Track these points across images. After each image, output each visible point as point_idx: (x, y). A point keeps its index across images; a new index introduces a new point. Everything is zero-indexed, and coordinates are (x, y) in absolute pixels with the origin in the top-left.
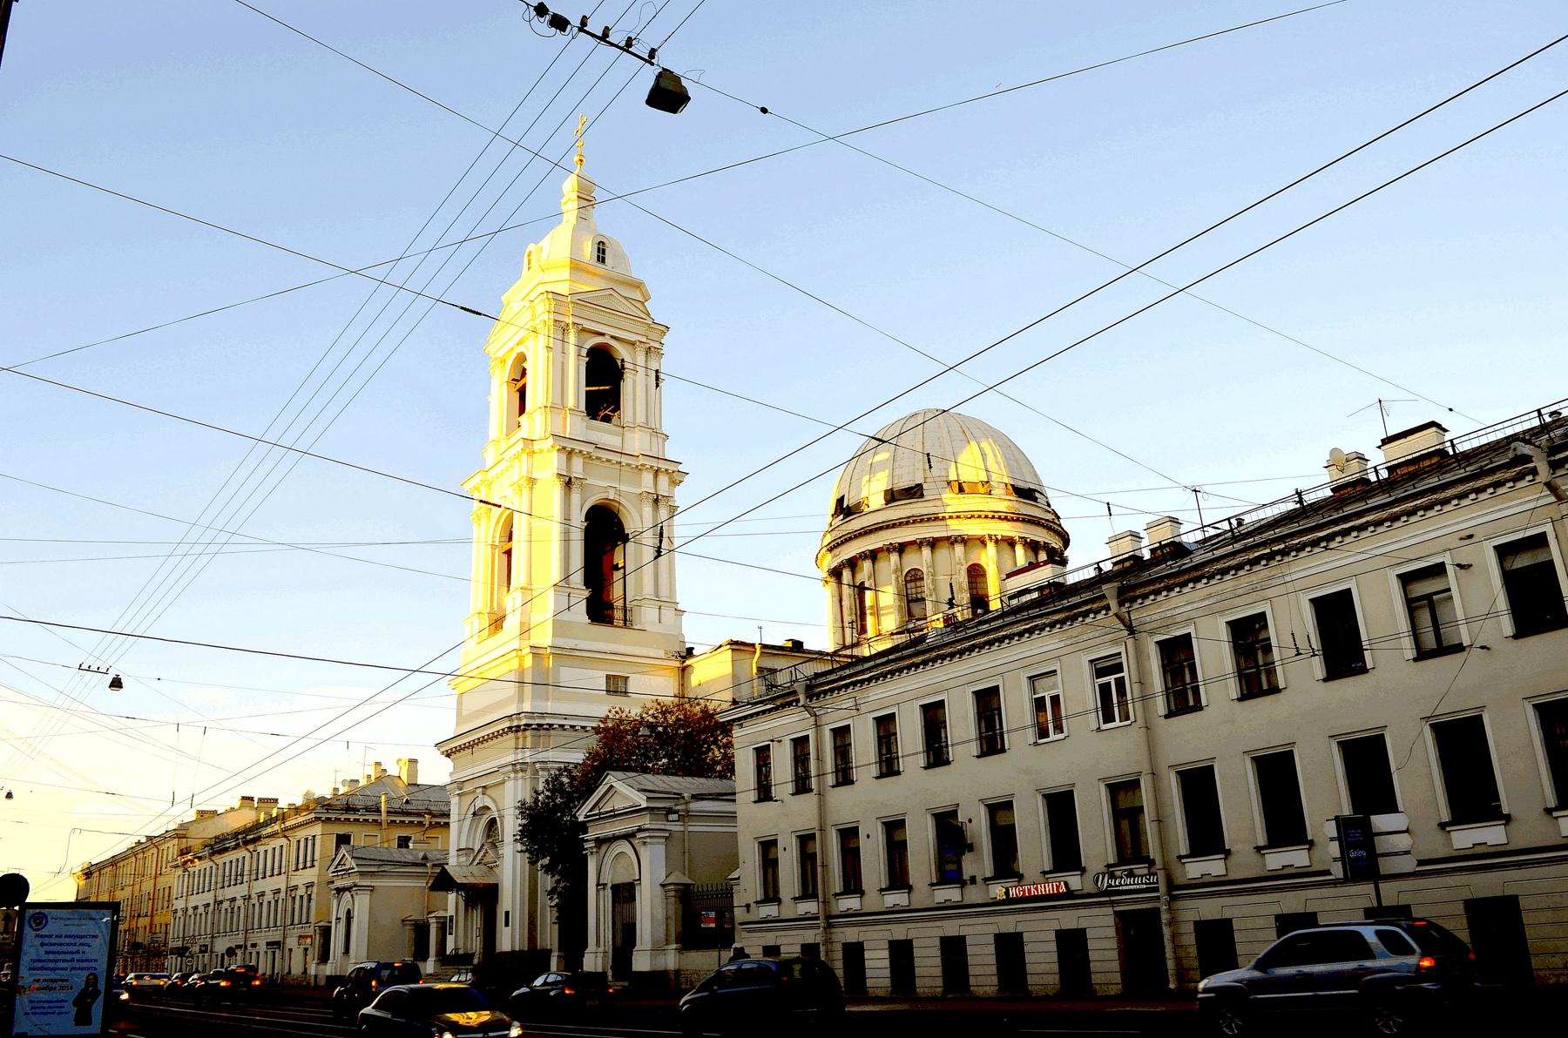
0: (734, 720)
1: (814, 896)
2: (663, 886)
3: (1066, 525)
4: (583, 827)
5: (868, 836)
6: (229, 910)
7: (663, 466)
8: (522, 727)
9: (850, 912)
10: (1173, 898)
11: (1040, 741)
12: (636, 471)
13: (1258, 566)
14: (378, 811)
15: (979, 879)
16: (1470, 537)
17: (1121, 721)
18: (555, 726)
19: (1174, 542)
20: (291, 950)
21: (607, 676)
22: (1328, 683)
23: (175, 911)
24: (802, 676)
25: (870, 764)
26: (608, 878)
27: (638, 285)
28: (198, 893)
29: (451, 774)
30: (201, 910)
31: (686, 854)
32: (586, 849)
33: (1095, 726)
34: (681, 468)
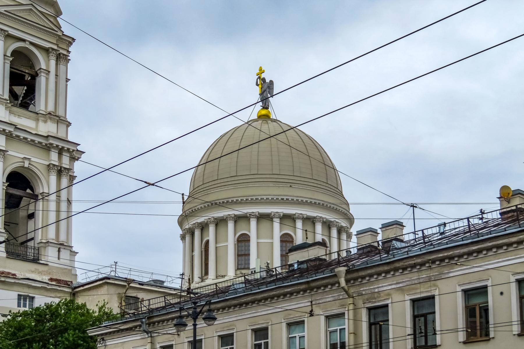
0: (98, 335)
3: (353, 210)
7: (66, 146)
12: (45, 147)
19: (370, 245)
21: (19, 295)
25: (406, 336)
34: (79, 148)
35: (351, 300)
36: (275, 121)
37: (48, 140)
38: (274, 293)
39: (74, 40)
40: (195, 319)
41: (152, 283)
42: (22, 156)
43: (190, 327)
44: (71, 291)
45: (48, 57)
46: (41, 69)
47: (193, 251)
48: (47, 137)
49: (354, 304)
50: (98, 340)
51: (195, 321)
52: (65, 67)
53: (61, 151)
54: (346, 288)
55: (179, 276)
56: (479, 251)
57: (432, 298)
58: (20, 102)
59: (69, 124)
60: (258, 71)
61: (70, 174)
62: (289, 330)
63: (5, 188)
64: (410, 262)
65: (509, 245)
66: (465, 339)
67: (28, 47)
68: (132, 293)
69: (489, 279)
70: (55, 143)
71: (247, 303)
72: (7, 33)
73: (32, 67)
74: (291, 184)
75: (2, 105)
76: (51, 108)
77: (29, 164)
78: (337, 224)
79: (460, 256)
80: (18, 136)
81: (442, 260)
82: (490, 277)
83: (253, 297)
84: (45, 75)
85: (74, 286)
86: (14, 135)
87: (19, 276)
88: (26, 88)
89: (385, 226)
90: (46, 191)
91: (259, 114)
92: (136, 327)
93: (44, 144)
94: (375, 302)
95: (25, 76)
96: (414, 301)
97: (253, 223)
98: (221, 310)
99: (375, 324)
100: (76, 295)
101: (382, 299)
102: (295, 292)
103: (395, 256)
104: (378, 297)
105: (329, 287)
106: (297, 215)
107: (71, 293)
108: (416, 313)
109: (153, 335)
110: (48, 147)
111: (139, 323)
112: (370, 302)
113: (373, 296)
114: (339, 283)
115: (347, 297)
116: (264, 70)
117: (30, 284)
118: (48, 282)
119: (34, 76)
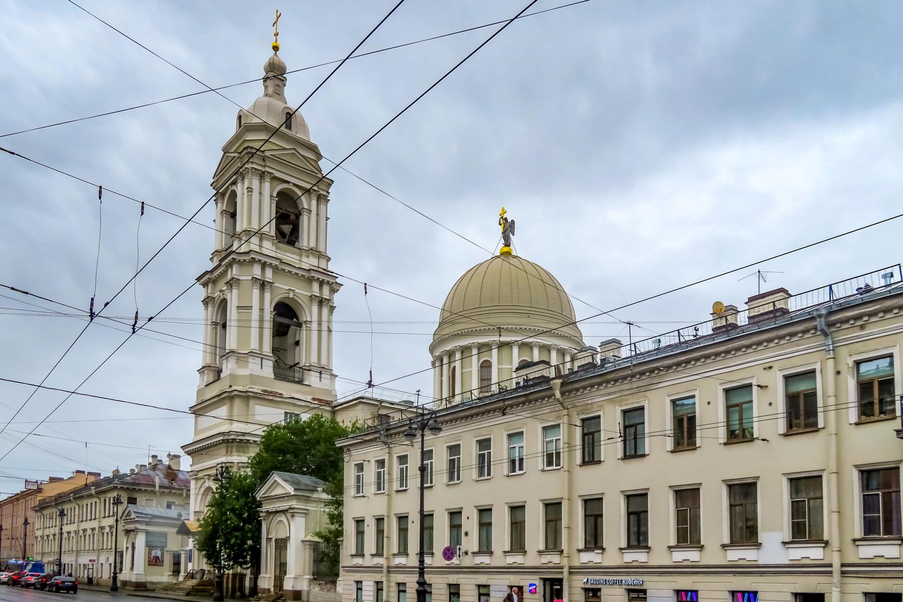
0: (345, 446)
1: (381, 555)
2: (303, 541)
4: (260, 505)
5: (413, 522)
6: (67, 538)
7: (326, 279)
8: (230, 440)
9: (400, 565)
10: (570, 573)
11: (510, 474)
13: (877, 317)
14: (154, 486)
15: (469, 553)
16: (770, 368)
17: (556, 466)
18: (251, 441)
20: (102, 564)
21: (285, 412)
22: (857, 426)
23: (37, 538)
24: (405, 417)
26: (273, 536)
27: (313, 149)
28: (67, 524)
29: (191, 466)
30: (89, 532)
31: (318, 524)
32: (261, 517)
33: (541, 467)
34: (338, 280)
35: (565, 412)
36: (515, 257)
37: (309, 274)
38: (496, 406)
39: (332, 181)
40: (423, 429)
41: (403, 404)
42: (288, 288)
43: (418, 439)
44: (331, 409)
45: (310, 197)
46: (303, 208)
47: (442, 376)
48: (309, 270)
49: (568, 415)
50: (345, 451)
51: (423, 432)
52: (325, 207)
53: (322, 283)
54: (561, 399)
55: (416, 393)
56: (688, 362)
57: (642, 408)
58: (287, 240)
59: (329, 259)
60: (500, 212)
61: (330, 304)
62: (509, 442)
63: (272, 316)
64: (622, 374)
65: (717, 354)
66: (673, 449)
67: (291, 188)
68: (383, 412)
69: (696, 389)
70: (316, 275)
71: (472, 416)
72: (272, 176)
73: (296, 207)
74: (529, 315)
75: (270, 241)
76: (313, 244)
77: (294, 295)
78: (571, 351)
79: (669, 367)
80: (284, 270)
81: (652, 371)
82: (698, 387)
83: (477, 410)
84: (307, 214)
85: (334, 405)
86: (280, 269)
87: (285, 395)
88: (291, 227)
89: (605, 343)
90: (309, 319)
91: (502, 252)
92: (376, 438)
93: (306, 277)
94: (588, 413)
95: (290, 215)
96: (625, 412)
97: (495, 352)
98: (449, 423)
99: (588, 434)
100: (336, 414)
101: (595, 410)
102: (515, 405)
103: (607, 368)
104: (590, 408)
105: (546, 399)
106: (534, 342)
107: (331, 411)
108: (626, 424)
109: (390, 446)
110: (311, 280)
111: (377, 435)
112: (583, 413)
113: (586, 408)
114: (554, 395)
115: (562, 409)
116: (506, 211)
117: (295, 402)
118: (311, 401)
119: (298, 215)
